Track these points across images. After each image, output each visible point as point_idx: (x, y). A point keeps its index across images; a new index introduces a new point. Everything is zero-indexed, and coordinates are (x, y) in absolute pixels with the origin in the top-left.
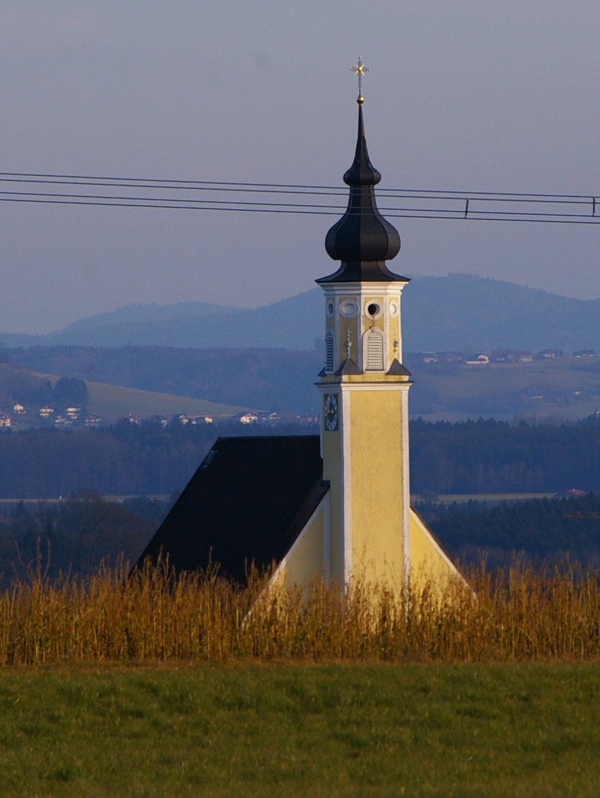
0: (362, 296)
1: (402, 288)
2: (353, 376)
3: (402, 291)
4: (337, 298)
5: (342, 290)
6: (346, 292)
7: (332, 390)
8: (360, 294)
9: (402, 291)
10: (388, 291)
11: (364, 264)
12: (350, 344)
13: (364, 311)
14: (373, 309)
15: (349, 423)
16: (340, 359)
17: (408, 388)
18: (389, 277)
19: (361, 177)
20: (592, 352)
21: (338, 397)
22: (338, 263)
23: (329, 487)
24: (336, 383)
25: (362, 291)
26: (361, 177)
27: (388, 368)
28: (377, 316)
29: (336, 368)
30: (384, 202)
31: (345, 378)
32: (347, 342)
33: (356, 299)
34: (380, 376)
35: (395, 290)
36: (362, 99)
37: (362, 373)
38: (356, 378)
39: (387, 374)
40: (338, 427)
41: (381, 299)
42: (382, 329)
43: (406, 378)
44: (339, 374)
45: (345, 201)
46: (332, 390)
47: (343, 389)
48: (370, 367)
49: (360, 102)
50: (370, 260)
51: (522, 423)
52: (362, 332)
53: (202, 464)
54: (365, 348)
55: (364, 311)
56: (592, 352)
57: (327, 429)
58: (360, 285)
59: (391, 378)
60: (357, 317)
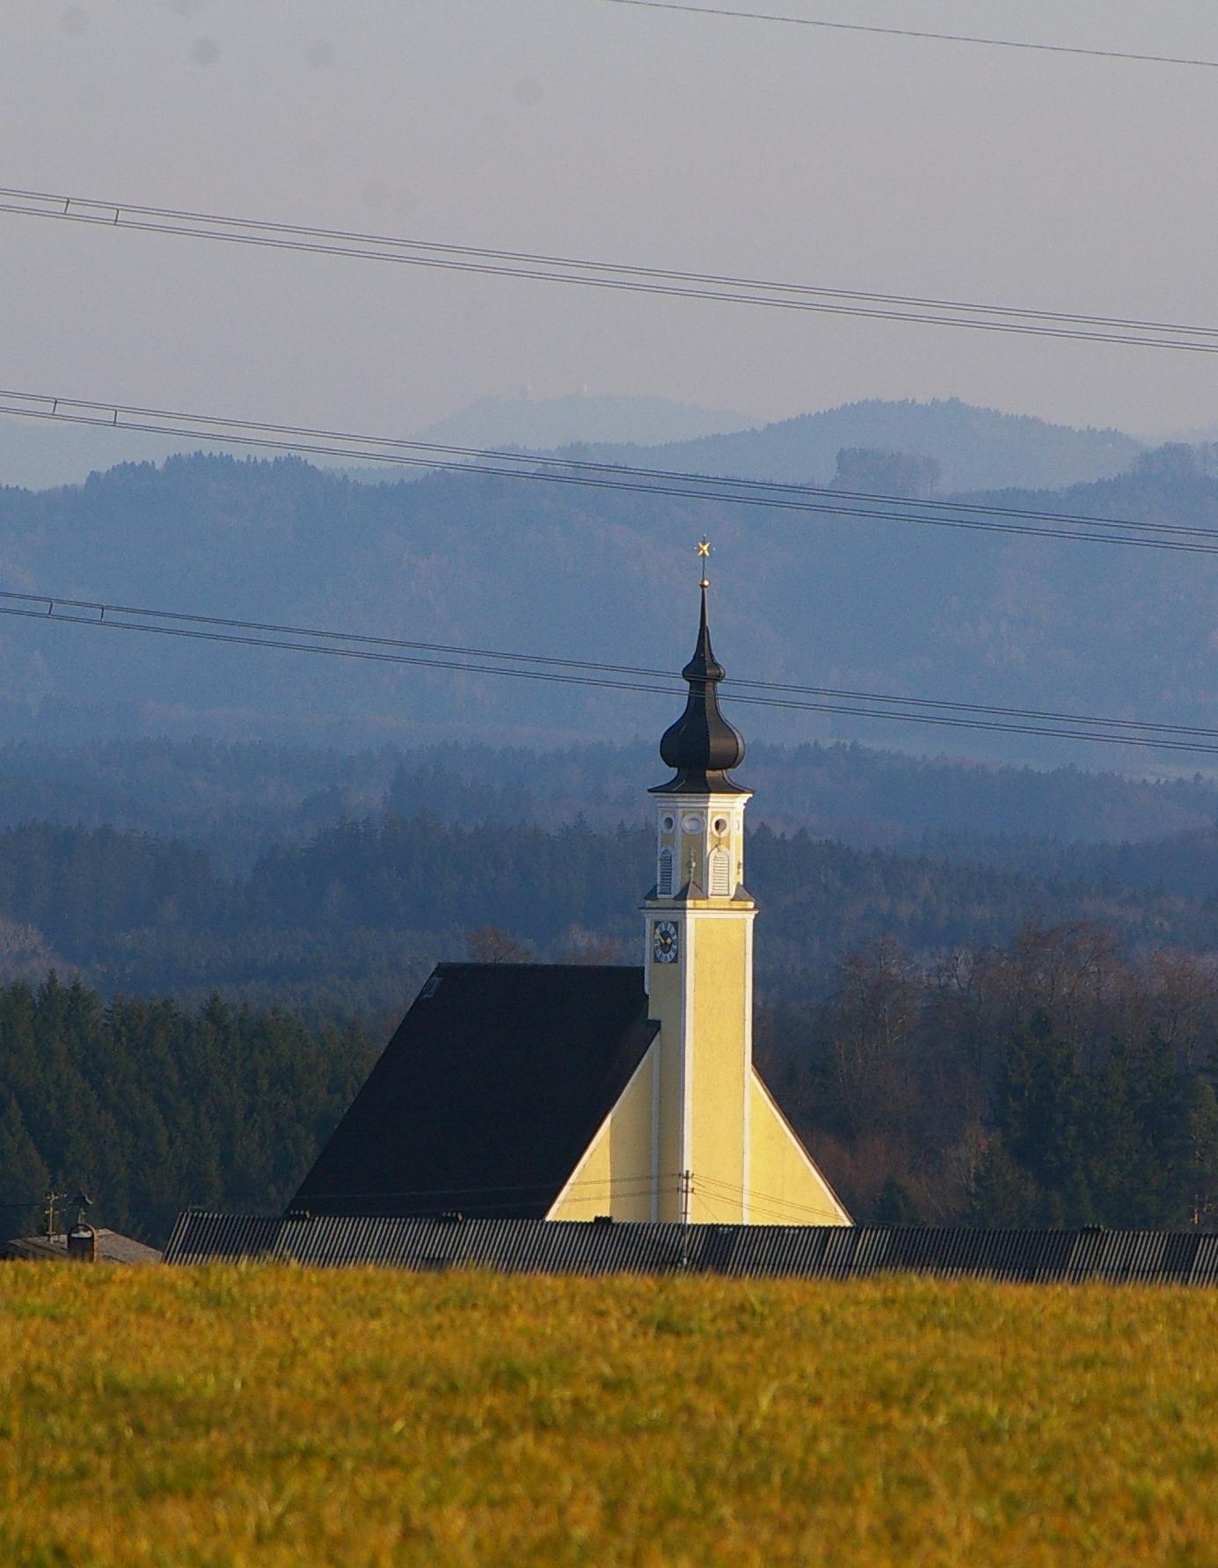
7: (672, 916)
11: (709, 773)
13: (711, 827)
14: (718, 824)
19: (701, 672)
21: (679, 926)
26: (701, 672)
27: (733, 892)
28: (724, 834)
29: (676, 890)
31: (689, 903)
34: (725, 901)
38: (701, 903)
40: (679, 959)
43: (751, 905)
44: (683, 896)
46: (672, 916)
49: (703, 586)
50: (714, 769)
51: (94, 475)
53: (422, 994)
57: (657, 960)
59: (736, 905)
60: (703, 834)
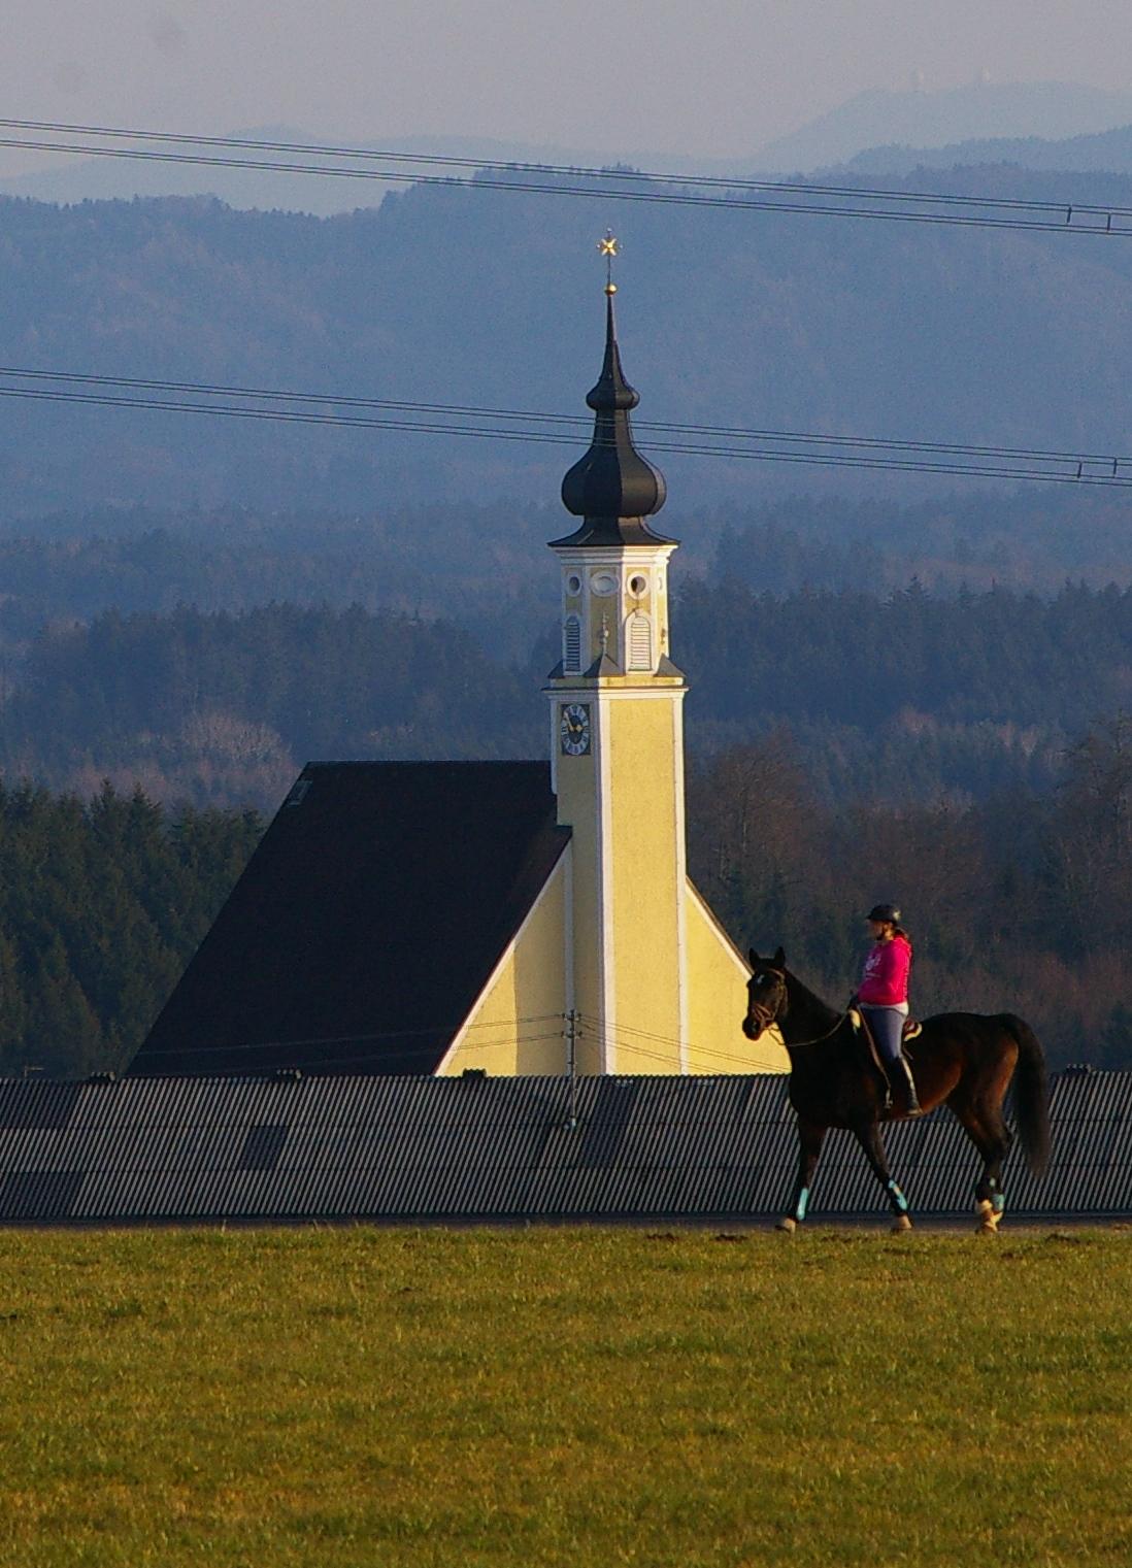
0: (624, 567)
1: (668, 554)
2: (613, 679)
3: (668, 558)
4: (587, 569)
5: (593, 557)
6: (605, 561)
8: (621, 564)
9: (668, 558)
10: (655, 559)
12: (606, 634)
13: (626, 587)
14: (635, 584)
15: (609, 744)
16: (579, 658)
17: (682, 695)
18: (655, 541)
19: (610, 398)
20: (509, 1023)
21: (590, 709)
22: (580, 519)
23: (571, 836)
24: (592, 688)
25: (624, 559)
26: (610, 398)
27: (656, 667)
28: (642, 595)
30: (643, 429)
31: (602, 681)
32: (602, 631)
33: (614, 571)
34: (646, 678)
35: (661, 556)
36: (613, 288)
37: (624, 674)
38: (617, 681)
39: (656, 675)
40: (591, 750)
41: (647, 570)
42: (649, 612)
44: (594, 673)
45: (588, 432)
47: (601, 696)
48: (635, 666)
50: (628, 516)
52: (624, 614)
54: (628, 640)
55: (626, 587)
56: (509, 1023)
57: (565, 752)
58: (622, 551)
59: (661, 681)
